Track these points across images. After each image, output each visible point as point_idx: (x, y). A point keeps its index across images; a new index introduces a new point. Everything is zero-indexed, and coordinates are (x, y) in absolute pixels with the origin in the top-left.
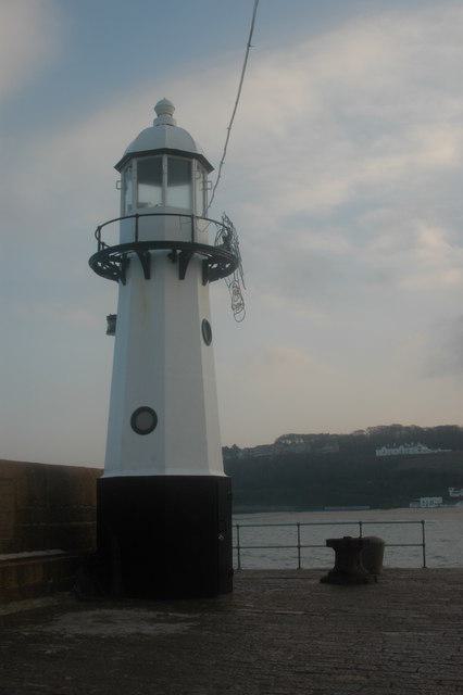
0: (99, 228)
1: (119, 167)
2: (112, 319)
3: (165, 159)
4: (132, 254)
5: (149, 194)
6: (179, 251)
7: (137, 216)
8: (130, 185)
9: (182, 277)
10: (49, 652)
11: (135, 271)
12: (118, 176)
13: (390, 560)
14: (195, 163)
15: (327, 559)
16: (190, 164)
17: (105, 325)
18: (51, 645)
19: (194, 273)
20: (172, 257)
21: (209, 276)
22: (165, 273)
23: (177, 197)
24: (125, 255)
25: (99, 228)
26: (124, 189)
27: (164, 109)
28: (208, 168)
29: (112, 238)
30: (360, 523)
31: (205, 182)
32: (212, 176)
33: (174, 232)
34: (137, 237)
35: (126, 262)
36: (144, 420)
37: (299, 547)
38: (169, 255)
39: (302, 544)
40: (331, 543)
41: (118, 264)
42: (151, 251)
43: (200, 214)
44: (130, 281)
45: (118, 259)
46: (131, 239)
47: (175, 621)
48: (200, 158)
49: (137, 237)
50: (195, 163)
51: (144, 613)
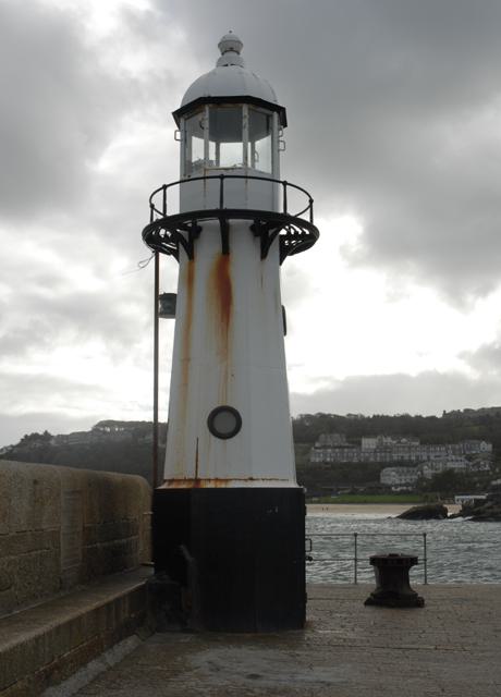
1: (178, 115)
9: (264, 255)
15: (368, 578)
16: (269, 117)
21: (286, 251)
24: (194, 224)
36: (225, 423)
45: (184, 227)
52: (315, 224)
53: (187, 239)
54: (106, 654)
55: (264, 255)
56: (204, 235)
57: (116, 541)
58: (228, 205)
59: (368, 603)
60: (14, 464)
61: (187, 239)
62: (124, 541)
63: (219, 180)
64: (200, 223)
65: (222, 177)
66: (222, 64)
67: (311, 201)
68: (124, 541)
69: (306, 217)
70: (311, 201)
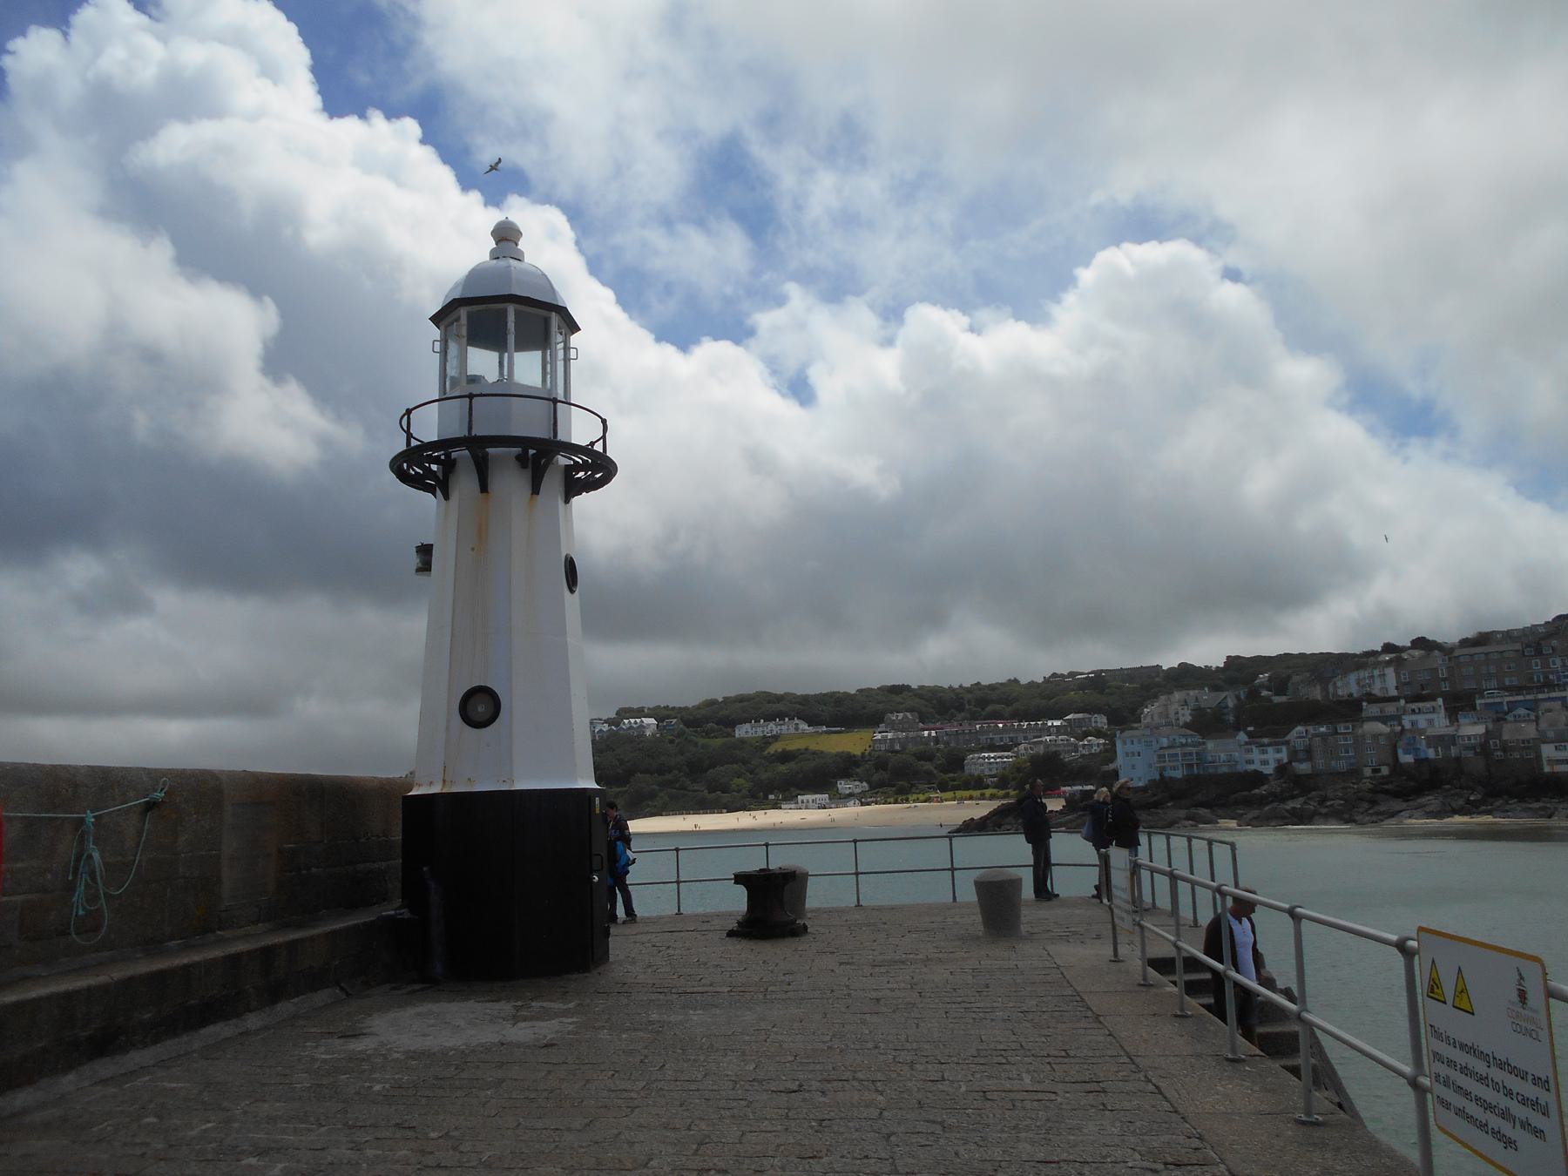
0: (409, 412)
1: (437, 319)
2: (425, 551)
3: (511, 310)
4: (461, 454)
5: (483, 362)
6: (531, 452)
7: (471, 396)
8: (453, 349)
9: (536, 490)
10: (377, 1088)
11: (465, 483)
12: (436, 333)
13: (816, 896)
14: (555, 319)
15: (737, 901)
16: (547, 321)
17: (414, 560)
18: (377, 1075)
19: (552, 483)
20: (522, 460)
21: (573, 488)
22: (510, 483)
23: (527, 368)
24: (448, 455)
25: (409, 412)
26: (444, 353)
27: (506, 236)
28: (573, 327)
29: (428, 428)
30: (677, 850)
31: (567, 349)
32: (575, 339)
33: (528, 423)
34: (470, 428)
35: (449, 466)
36: (481, 709)
37: (678, 882)
38: (518, 458)
39: (854, 876)
40: (740, 879)
41: (434, 467)
42: (490, 450)
43: (561, 397)
44: (455, 495)
45: (437, 461)
46: (457, 430)
47: (545, 1015)
48: (563, 312)
49: (470, 428)
50: (555, 319)
51: (506, 1007)
52: (426, 441)
53: (440, 475)
54: (267, 1008)
55: (536, 490)
56: (460, 466)
57: (361, 867)
58: (478, 431)
59: (731, 934)
60: (1043, 856)
61: (440, 475)
62: (383, 865)
63: (468, 399)
64: (454, 455)
65: (855, 841)
66: (495, 255)
67: (604, 422)
68: (383, 865)
69: (598, 447)
70: (604, 422)
